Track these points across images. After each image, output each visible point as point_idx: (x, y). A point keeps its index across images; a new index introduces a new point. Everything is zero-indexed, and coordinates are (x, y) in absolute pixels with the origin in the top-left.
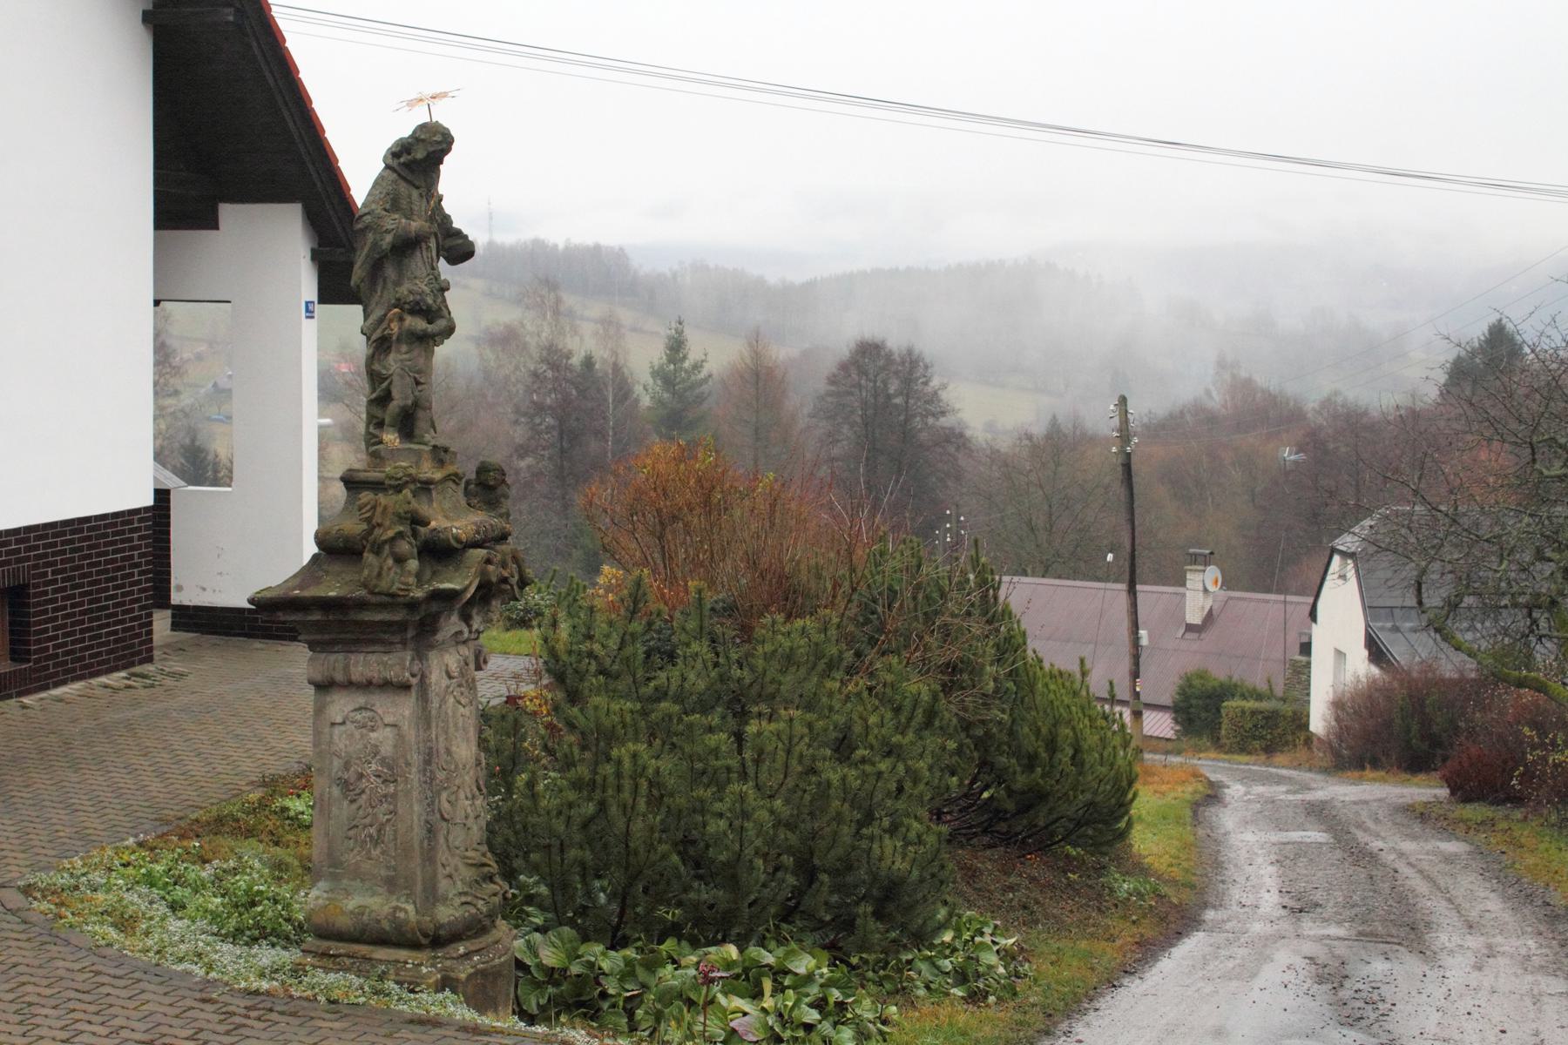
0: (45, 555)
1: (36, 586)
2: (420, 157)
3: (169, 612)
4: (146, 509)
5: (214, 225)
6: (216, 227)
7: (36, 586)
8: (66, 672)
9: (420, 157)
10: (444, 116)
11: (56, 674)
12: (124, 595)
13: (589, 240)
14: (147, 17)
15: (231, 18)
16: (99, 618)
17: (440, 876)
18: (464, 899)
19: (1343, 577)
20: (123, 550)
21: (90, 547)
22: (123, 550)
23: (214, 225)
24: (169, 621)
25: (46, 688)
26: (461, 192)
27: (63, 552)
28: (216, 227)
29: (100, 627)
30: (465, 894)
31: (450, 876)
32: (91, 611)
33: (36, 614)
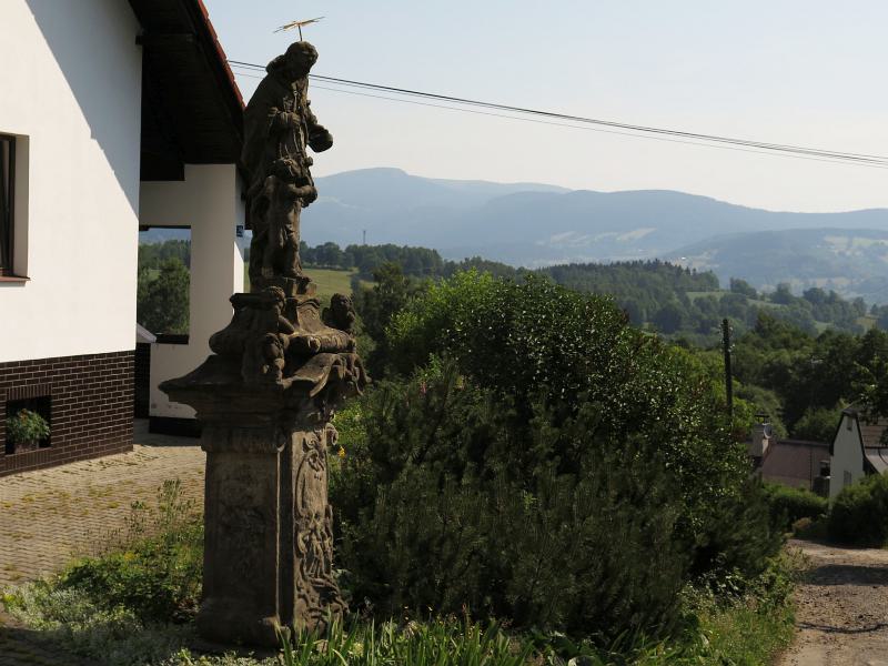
0: (62, 378)
1: (55, 397)
2: (294, 66)
3: (148, 421)
4: (130, 352)
5: (180, 176)
6: (183, 179)
7: (55, 397)
8: (74, 454)
9: (294, 66)
10: (310, 37)
11: (67, 455)
12: (114, 406)
13: (417, 246)
14: (139, 41)
15: (191, 40)
16: (97, 421)
17: (296, 597)
18: (313, 614)
19: (850, 429)
20: (114, 378)
21: (92, 375)
22: (114, 378)
23: (180, 176)
24: (147, 426)
25: (60, 464)
26: (322, 100)
27: (74, 377)
28: (183, 179)
29: (98, 426)
30: (316, 610)
31: (304, 597)
32: (92, 415)
33: (56, 415)
